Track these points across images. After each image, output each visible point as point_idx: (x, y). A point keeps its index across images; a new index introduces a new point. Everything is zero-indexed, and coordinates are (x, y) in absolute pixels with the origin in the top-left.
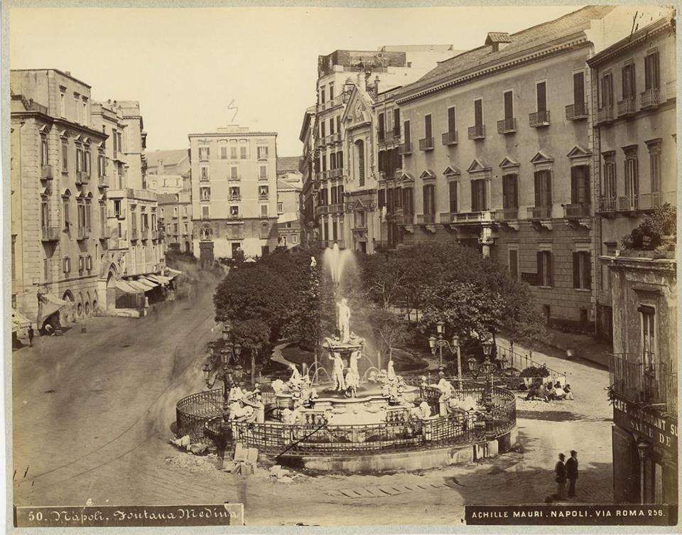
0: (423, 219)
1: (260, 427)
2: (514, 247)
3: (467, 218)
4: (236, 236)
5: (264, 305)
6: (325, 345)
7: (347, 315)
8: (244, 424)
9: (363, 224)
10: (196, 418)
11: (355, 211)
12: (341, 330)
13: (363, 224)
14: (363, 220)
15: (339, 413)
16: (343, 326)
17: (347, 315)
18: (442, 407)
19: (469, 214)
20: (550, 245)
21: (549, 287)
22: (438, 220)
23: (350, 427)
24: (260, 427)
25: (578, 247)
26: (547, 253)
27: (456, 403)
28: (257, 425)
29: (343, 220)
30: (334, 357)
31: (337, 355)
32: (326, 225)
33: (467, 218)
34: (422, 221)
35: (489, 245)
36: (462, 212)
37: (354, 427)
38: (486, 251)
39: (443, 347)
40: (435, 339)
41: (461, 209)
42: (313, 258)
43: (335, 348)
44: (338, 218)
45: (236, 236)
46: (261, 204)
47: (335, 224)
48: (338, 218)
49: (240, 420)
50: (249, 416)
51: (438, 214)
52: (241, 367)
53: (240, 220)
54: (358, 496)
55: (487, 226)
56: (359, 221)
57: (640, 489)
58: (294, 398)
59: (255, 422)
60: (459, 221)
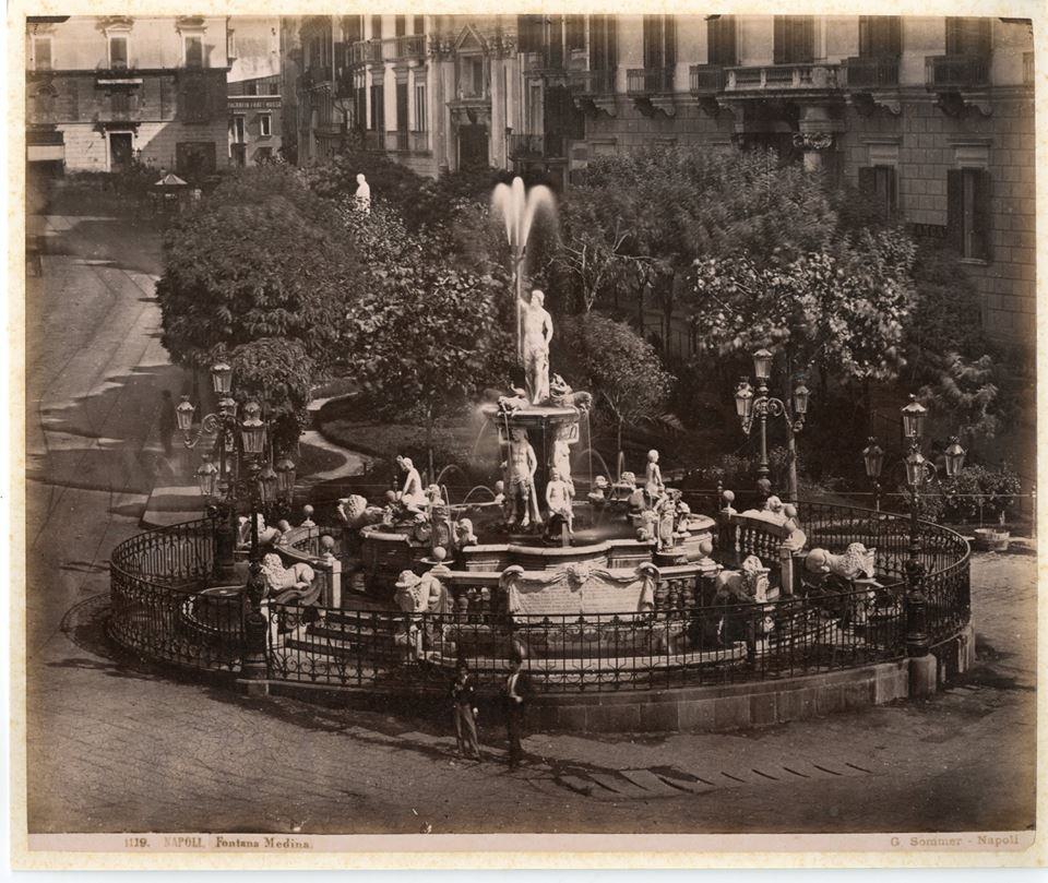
4: (121, 116)
5: (292, 305)
9: (478, 88)
10: (157, 590)
13: (478, 88)
14: (478, 79)
17: (545, 332)
20: (984, 154)
21: (980, 261)
22: (623, 85)
23: (576, 619)
25: (875, 157)
26: (977, 174)
29: (424, 79)
30: (512, 438)
31: (521, 434)
32: (378, 91)
42: (361, 178)
44: (411, 74)
45: (121, 116)
46: (185, 35)
47: (402, 91)
48: (411, 74)
50: (304, 589)
54: (738, 783)
55: (812, 102)
56: (467, 83)
59: (317, 604)
60: (742, 88)
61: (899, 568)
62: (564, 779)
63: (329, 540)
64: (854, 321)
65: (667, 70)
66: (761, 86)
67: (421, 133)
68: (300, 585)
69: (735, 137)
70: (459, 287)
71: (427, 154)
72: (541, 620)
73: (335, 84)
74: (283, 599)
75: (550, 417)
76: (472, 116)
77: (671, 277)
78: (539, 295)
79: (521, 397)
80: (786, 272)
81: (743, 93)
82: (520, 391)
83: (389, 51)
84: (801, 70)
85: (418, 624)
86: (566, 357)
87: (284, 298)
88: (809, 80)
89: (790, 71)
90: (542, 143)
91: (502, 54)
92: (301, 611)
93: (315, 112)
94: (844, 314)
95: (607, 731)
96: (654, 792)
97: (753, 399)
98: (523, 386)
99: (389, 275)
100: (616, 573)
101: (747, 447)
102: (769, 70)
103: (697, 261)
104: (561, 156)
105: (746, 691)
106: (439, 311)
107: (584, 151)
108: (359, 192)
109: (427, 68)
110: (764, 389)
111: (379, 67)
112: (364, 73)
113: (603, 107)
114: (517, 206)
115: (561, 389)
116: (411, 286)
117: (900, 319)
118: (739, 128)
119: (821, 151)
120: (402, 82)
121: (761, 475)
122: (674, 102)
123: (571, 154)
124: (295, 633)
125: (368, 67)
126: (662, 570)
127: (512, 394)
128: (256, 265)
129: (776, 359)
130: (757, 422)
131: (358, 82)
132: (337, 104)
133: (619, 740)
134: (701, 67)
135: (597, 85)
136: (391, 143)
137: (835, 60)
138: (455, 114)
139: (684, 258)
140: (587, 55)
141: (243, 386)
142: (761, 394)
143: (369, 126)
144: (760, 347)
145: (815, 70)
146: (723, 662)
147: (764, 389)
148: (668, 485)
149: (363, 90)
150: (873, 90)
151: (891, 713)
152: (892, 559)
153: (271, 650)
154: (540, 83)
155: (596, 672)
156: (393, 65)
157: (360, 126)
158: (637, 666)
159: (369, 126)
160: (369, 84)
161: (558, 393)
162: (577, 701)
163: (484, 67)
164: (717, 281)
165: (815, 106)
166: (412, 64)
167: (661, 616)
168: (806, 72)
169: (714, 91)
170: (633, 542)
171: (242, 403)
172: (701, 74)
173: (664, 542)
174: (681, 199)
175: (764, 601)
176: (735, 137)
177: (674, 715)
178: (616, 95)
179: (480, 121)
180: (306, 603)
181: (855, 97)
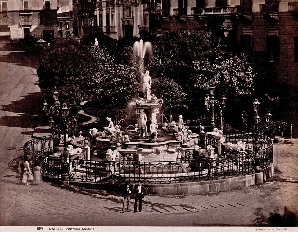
0: (177, 12)
3: (213, 11)
7: (149, 82)
11: (123, 6)
14: (130, 12)
17: (149, 82)
19: (214, 9)
22: (172, 13)
23: (159, 163)
24: (87, 163)
28: (85, 162)
30: (140, 112)
32: (101, 15)
33: (213, 11)
34: (176, 13)
37: (161, 163)
42: (96, 40)
44: (110, 11)
47: (108, 15)
48: (110, 11)
49: (73, 158)
50: (79, 155)
51: (172, 9)
53: (30, 11)
56: (127, 13)
57: (79, 183)
59: (83, 159)
63: (87, 141)
64: (239, 79)
67: (113, 27)
68: (78, 154)
70: (124, 70)
71: (115, 33)
74: (73, 158)
76: (128, 22)
79: (142, 100)
80: (219, 65)
82: (142, 99)
85: (113, 165)
86: (156, 90)
92: (79, 161)
94: (236, 76)
96: (181, 212)
97: (209, 101)
109: (115, 9)
111: (101, 9)
112: (97, 10)
114: (141, 47)
116: (110, 70)
126: (183, 149)
131: (95, 13)
132: (89, 19)
136: (105, 30)
138: (123, 22)
142: (212, 99)
147: (213, 98)
152: (250, 145)
153: (70, 172)
156: (105, 8)
160: (98, 13)
162: (160, 186)
163: (132, 8)
170: (175, 141)
178: (187, 15)
180: (80, 159)
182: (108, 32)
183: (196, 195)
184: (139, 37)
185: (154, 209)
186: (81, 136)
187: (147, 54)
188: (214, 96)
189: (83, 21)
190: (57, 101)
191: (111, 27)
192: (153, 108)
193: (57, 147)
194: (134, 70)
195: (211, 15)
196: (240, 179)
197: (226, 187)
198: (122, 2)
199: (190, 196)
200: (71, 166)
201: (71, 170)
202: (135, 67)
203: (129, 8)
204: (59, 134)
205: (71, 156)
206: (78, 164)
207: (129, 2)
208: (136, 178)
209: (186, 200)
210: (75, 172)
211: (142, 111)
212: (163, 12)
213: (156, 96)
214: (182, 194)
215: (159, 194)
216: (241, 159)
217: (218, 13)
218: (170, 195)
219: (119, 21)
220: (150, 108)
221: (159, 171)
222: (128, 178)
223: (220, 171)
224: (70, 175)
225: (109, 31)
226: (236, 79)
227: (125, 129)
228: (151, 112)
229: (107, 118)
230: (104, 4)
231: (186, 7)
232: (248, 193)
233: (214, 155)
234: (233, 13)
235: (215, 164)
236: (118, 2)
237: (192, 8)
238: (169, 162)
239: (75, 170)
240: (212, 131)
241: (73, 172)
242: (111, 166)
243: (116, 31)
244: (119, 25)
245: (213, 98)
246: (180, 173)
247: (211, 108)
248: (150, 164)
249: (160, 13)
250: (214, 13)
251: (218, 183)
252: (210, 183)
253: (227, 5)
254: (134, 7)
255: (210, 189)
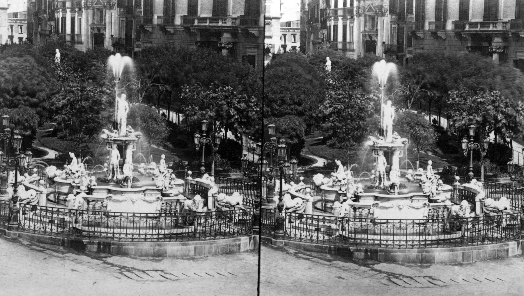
1: (41, 210)
2: (252, 52)
3: (479, 26)
5: (300, 104)
6: (104, 136)
7: (126, 109)
8: (28, 206)
11: (93, 8)
12: (118, 122)
15: (387, 208)
16: (387, 127)
17: (126, 109)
18: (210, 200)
22: (427, 27)
27: (490, 202)
29: (81, 15)
30: (378, 155)
32: (336, 27)
33: (479, 26)
34: (433, 27)
35: (228, 49)
36: (473, 21)
37: (402, 221)
38: (224, 52)
39: (206, 144)
40: (467, 141)
41: (201, 13)
42: (57, 50)
43: (380, 147)
47: (345, 27)
50: (33, 199)
51: (155, 17)
52: (31, 153)
58: (340, 192)
59: (303, 213)
61: (251, 202)
62: (392, 279)
63: (308, 190)
64: (507, 116)
65: (172, 16)
66: (478, 29)
67: (351, 43)
68: (297, 206)
69: (468, 48)
70: (361, 99)
71: (353, 51)
72: (386, 221)
73: (320, 24)
74: (24, 202)
75: (126, 140)
76: (99, 30)
77: (171, 92)
78: (124, 96)
79: (116, 133)
80: (215, 92)
81: (471, 31)
82: (115, 131)
83: (340, 13)
84: (493, 23)
85: (340, 221)
86: (400, 127)
87: (297, 101)
88: (496, 27)
89: (489, 23)
90: (396, 48)
91: (383, 15)
92: (297, 215)
93: (312, 35)
94: (503, 113)
95: (141, 256)
96: (425, 285)
97: (200, 138)
98: (117, 129)
99: (336, 94)
100: (148, 198)
101: (465, 161)
102: (481, 23)
103: (450, 92)
104: (403, 52)
105: (193, 244)
106: (87, 100)
107: (140, 45)
108: (327, 64)
109: (354, 19)
110: (205, 134)
111: (336, 19)
112: (59, 12)
113: (148, 29)
114: (118, 63)
115: (397, 137)
116: (343, 98)
117: (256, 112)
118: (198, 39)
119: (228, 49)
120: (73, 16)
121: (470, 171)
122: (445, 34)
123: (135, 46)
124: (294, 224)
125: (332, 18)
126: (431, 204)
127: (112, 132)
128: (287, 89)
129: (478, 128)
130: (469, 151)
131: (56, 15)
132: (321, 31)
133: (145, 260)
134: (456, 22)
135: (417, 27)
136: (68, 38)
137: (506, 20)
138: (364, 36)
139: (445, 90)
140: (414, 16)
141: (280, 133)
142: (203, 136)
143: (60, 31)
144: (472, 124)
145: (498, 24)
146: (185, 233)
147: (472, 139)
148: (168, 168)
149: (330, 27)
150: (249, 28)
151: (515, 260)
152: (517, 203)
153: (20, 221)
154: (124, 19)
155: (372, 240)
156: (70, 10)
157: (57, 32)
158: (421, 239)
159: (60, 31)
160: (61, 16)
161: (130, 132)
162: (399, 252)
163: (376, 19)
164: (457, 99)
165: (227, 32)
166: (349, 17)
167: (163, 215)
168: (495, 24)
169: (189, 25)
170: (422, 194)
171: (279, 139)
172: (455, 24)
173: (433, 194)
174: (446, 71)
175: (201, 211)
176: (468, 48)
177: (434, 258)
178: (424, 31)
179: (101, 32)
180: (300, 212)
181: (513, 33)
182: (345, 49)
183: (446, 264)
184: (112, 50)
185: (390, 281)
186: (302, 183)
187: (390, 79)
188: (474, 137)
189: (41, 26)
190: (273, 136)
191: (77, 35)
192: (394, 150)
193: (271, 196)
194: (374, 100)
195: (206, 26)
196: (235, 241)
197: (484, 256)
198: (92, 3)
199: (438, 266)
200: (287, 221)
201: (287, 226)
202: (374, 95)
203: (373, 18)
204: (275, 180)
205: (287, 209)
206: (295, 219)
207: (101, 4)
208: (96, 232)
209: (431, 271)
210: (26, 221)
211: (381, 153)
212: (144, 19)
213: (399, 134)
214: (159, 256)
215: (399, 261)
216: (504, 220)
217: (486, 29)
218: (412, 263)
219: (359, 34)
220: (391, 149)
221: (132, 225)
222: (359, 239)
223: (477, 235)
224: (285, 233)
225: (346, 48)
226: (236, 112)
227: (91, 169)
228: (126, 148)
229: (70, 153)
230: (68, 4)
231: (174, 16)
232: (511, 265)
233: (203, 208)
234: (234, 25)
235: (471, 225)
236: (86, 4)
237: (181, 16)
238: (412, 221)
239: (26, 219)
240: (201, 177)
241: (23, 221)
242: (338, 223)
243: (355, 48)
244: (359, 41)
245: (472, 139)
246: (426, 235)
247: (201, 148)
248: (387, 222)
249: (140, 21)
250: (210, 25)
251: (472, 250)
252: (464, 250)
253: (497, 20)
254: (107, 11)
255: (463, 257)
